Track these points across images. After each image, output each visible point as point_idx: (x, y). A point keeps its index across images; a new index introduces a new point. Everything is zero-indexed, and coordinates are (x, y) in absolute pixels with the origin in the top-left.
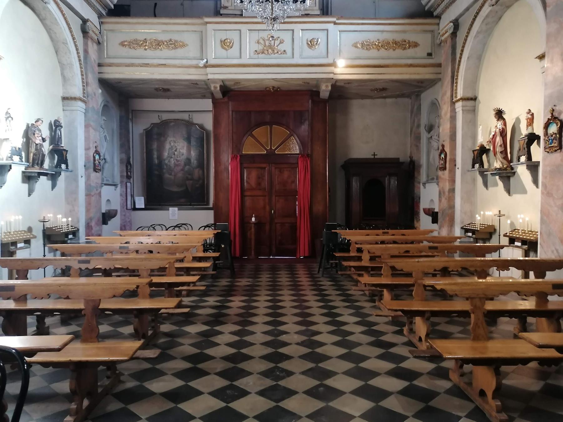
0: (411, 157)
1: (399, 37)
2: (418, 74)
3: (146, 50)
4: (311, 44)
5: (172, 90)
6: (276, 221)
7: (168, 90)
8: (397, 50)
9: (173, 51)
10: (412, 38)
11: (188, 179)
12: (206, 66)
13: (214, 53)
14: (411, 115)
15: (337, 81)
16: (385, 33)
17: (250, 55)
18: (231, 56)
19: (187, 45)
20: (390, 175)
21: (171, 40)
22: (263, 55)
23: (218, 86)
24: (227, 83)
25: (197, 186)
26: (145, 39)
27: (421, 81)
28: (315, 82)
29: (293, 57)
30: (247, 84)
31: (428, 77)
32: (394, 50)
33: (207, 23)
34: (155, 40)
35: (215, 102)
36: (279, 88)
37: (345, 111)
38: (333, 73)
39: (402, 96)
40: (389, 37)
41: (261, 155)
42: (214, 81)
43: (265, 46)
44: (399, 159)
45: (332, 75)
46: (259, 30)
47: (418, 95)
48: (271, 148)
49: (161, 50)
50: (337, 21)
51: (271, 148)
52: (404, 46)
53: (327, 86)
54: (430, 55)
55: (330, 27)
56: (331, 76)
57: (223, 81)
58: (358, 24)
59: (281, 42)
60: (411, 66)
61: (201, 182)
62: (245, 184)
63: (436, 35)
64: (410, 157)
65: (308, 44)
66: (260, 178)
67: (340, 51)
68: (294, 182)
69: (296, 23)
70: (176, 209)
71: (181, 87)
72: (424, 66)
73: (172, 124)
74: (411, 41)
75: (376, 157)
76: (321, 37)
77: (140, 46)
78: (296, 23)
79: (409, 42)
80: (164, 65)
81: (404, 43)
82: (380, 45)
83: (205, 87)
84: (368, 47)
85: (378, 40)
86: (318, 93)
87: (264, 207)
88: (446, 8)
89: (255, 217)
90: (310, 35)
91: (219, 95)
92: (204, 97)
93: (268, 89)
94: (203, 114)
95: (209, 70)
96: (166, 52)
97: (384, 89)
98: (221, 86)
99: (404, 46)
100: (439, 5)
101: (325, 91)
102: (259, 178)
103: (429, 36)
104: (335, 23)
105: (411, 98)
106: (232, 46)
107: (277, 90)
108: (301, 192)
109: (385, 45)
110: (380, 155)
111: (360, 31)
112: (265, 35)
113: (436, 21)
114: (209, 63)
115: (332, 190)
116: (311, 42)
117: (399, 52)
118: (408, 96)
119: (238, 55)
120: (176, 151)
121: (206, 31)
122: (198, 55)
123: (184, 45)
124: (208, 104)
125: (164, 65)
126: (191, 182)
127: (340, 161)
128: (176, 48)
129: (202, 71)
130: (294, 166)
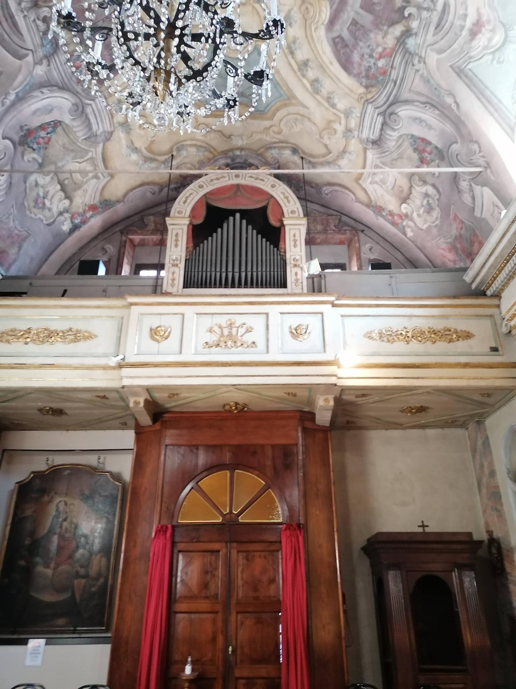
0: (490, 533)
1: (439, 325)
2: (481, 378)
3: (26, 343)
4: (296, 333)
5: (67, 411)
6: (237, 673)
7: (59, 412)
8: (438, 343)
9: (72, 345)
10: (461, 325)
11: (78, 576)
12: (120, 366)
13: (138, 346)
14: (474, 457)
15: (344, 390)
16: (415, 319)
17: (196, 349)
18: (167, 350)
19: (96, 336)
20: (462, 567)
21: (70, 329)
22: (218, 349)
23: (142, 401)
24: (157, 395)
25: (94, 589)
26: (29, 329)
27: (487, 393)
28: (306, 394)
29: (268, 352)
30: (192, 396)
31: (498, 383)
32: (434, 342)
33: (132, 304)
34: (46, 329)
35: (140, 432)
36: (245, 405)
37: (360, 449)
38: (336, 376)
39: (452, 423)
40: (424, 324)
41: (213, 524)
42: (133, 390)
43: (222, 335)
44: (470, 534)
45: (335, 378)
46: (213, 314)
47: (480, 421)
48: (231, 512)
49: (52, 343)
50: (336, 302)
51: (231, 512)
52: (449, 337)
53: (326, 400)
54: (495, 349)
55: (327, 309)
56: (333, 380)
57: (148, 390)
58: (370, 306)
59: (248, 331)
60: (466, 365)
61: (102, 580)
62: (179, 586)
63: (498, 321)
64: (488, 532)
65: (291, 332)
66: (207, 572)
67: (345, 343)
68: (273, 581)
69: (272, 303)
70: (42, 641)
71: (82, 405)
72: (490, 366)
73: (66, 473)
74: (459, 330)
75: (427, 530)
76: (313, 322)
77: (18, 339)
78: (272, 303)
79: (456, 332)
80: (52, 366)
81: (447, 333)
82: (409, 334)
83: (122, 404)
84: (390, 338)
85: (405, 328)
86: (311, 416)
87: (214, 639)
88: (509, 280)
89: (193, 663)
90: (294, 321)
91: (146, 420)
92: (124, 426)
93: (227, 408)
94: (115, 450)
95: (125, 371)
96: (59, 347)
97: (422, 409)
98: (146, 401)
99: (449, 337)
100: (495, 278)
101: (324, 410)
102: (206, 572)
103: (487, 323)
104: (334, 305)
105: (467, 429)
106: (168, 336)
107: (242, 410)
108: (288, 603)
109: (419, 335)
110: (433, 527)
111: (374, 316)
112: (223, 321)
113: (495, 301)
114: (127, 361)
115: (349, 599)
116: (296, 330)
117: (442, 346)
118: (463, 425)
119: (177, 349)
120: (65, 520)
121: (129, 315)
122: (112, 349)
123: (90, 337)
124: (127, 438)
125: (52, 366)
126: (83, 581)
127: (359, 540)
128: (76, 340)
129: (115, 373)
130: (273, 548)
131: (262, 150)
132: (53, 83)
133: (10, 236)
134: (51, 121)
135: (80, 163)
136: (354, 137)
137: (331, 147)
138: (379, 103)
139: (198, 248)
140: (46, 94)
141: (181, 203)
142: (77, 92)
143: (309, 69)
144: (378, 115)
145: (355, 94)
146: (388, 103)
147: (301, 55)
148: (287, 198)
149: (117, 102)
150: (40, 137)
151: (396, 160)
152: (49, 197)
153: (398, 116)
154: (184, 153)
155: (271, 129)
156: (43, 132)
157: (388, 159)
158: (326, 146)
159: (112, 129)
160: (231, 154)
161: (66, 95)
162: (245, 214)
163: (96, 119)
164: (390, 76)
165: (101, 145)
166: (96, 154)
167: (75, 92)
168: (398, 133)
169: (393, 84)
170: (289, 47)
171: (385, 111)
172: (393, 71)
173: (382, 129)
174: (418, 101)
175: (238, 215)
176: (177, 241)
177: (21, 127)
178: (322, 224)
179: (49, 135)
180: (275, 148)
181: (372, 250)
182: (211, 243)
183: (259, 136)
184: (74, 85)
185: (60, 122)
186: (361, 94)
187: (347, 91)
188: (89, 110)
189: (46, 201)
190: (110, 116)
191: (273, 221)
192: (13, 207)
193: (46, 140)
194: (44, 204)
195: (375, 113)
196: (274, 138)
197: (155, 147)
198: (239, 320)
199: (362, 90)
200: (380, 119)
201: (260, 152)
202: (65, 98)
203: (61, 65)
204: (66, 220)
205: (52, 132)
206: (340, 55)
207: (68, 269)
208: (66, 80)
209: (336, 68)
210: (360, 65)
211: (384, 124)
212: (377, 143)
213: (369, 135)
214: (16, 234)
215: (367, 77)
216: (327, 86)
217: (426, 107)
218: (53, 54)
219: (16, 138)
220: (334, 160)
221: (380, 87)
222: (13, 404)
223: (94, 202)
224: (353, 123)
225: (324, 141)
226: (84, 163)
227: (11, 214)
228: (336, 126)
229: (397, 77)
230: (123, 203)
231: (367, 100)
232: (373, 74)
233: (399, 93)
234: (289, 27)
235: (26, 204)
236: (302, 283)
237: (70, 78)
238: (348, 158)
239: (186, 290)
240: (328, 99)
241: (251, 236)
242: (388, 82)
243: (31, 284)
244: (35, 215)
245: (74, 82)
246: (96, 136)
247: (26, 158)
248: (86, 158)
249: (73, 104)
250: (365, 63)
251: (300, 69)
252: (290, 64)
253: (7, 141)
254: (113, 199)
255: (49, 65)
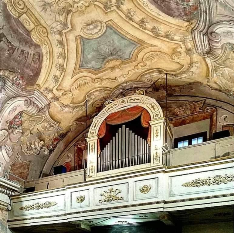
4: (144, 190)
90: (141, 184)
112: (107, 189)
131: (139, 78)
132: (11, 97)
133: (22, 166)
134: (19, 113)
135: (40, 124)
136: (193, 53)
137: (182, 63)
138: (201, 28)
139: (103, 150)
140: (10, 103)
141: (93, 128)
142: (24, 95)
143: (147, 24)
144: (203, 36)
145: (183, 27)
146: (207, 27)
147: (138, 17)
148: (153, 107)
149: (45, 89)
150: (16, 122)
151: (225, 61)
152: (33, 144)
153: (216, 33)
154: (93, 97)
155: (139, 65)
156: (17, 119)
157: (221, 61)
158: (178, 63)
159: (49, 103)
160: (121, 87)
161: (19, 99)
162: (128, 125)
163: (39, 101)
164: (200, 9)
165: (47, 112)
166: (47, 117)
167: (23, 95)
168: (221, 44)
169: (205, 14)
170: (127, 17)
171: (207, 32)
172: (202, 5)
173: (209, 44)
174: (225, 21)
175: (124, 126)
176: (92, 149)
177: (6, 122)
178: (191, 110)
179: (20, 119)
180: (146, 74)
181: (226, 119)
182: (110, 146)
183: (133, 72)
184: (20, 92)
185: (22, 111)
186: (187, 26)
187: (177, 27)
188: (33, 100)
189: (32, 146)
190: (45, 97)
191: (144, 125)
192: (18, 154)
193: (20, 122)
194: (31, 147)
195: (201, 35)
196: (143, 69)
197: (75, 101)
198: (115, 188)
199: (186, 24)
200: (206, 38)
201: (138, 79)
202: (20, 100)
203: (10, 87)
204: (45, 149)
205: (21, 117)
206: (162, 7)
207: (231, 28)
208: (16, 93)
209: (163, 16)
210: (178, 9)
211: (209, 40)
212: (210, 52)
213: (203, 49)
214: (24, 164)
215: (186, 14)
216: (163, 29)
217: (231, 23)
218: (5, 85)
219: (7, 128)
220: (188, 69)
221: (197, 18)
222: (37, 229)
223: (55, 137)
224: (190, 45)
225: (176, 61)
226: (43, 123)
227: (18, 157)
228: (179, 50)
229: (206, 8)
230: (71, 132)
231: (192, 29)
232: (189, 12)
233: (211, 19)
234: (122, 6)
235: (23, 151)
236: (160, 158)
237: (18, 91)
238: (196, 66)
239: (98, 173)
240: (167, 36)
241: (128, 138)
242: (201, 13)
243: (35, 183)
244: (30, 153)
245: (20, 91)
246: (43, 109)
247: (14, 133)
248: (42, 121)
249: (25, 101)
250: (181, 6)
251: (141, 26)
252: (133, 26)
253: (4, 131)
254: (65, 131)
255: (5, 91)
